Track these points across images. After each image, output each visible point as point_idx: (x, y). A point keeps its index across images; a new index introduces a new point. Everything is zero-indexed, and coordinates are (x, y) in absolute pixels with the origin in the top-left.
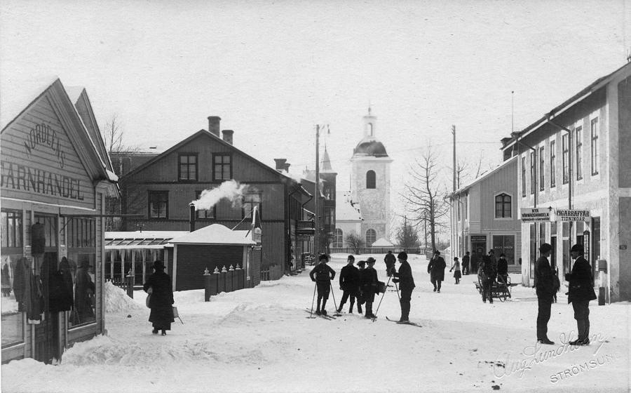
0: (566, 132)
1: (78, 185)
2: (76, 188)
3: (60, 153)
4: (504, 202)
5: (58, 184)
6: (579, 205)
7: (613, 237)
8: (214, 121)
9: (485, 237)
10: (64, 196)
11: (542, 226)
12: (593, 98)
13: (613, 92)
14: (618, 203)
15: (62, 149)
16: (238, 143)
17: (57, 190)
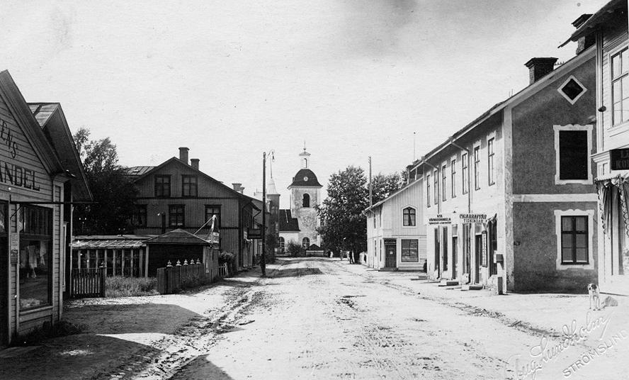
0: (466, 152)
1: (34, 176)
2: (29, 178)
3: (12, 143)
4: (409, 214)
5: (8, 172)
6: (475, 211)
7: (508, 234)
8: (184, 151)
9: (395, 241)
10: (16, 184)
11: (445, 230)
12: (488, 124)
13: (508, 118)
14: (512, 207)
15: (14, 140)
16: (202, 168)
17: (8, 177)
